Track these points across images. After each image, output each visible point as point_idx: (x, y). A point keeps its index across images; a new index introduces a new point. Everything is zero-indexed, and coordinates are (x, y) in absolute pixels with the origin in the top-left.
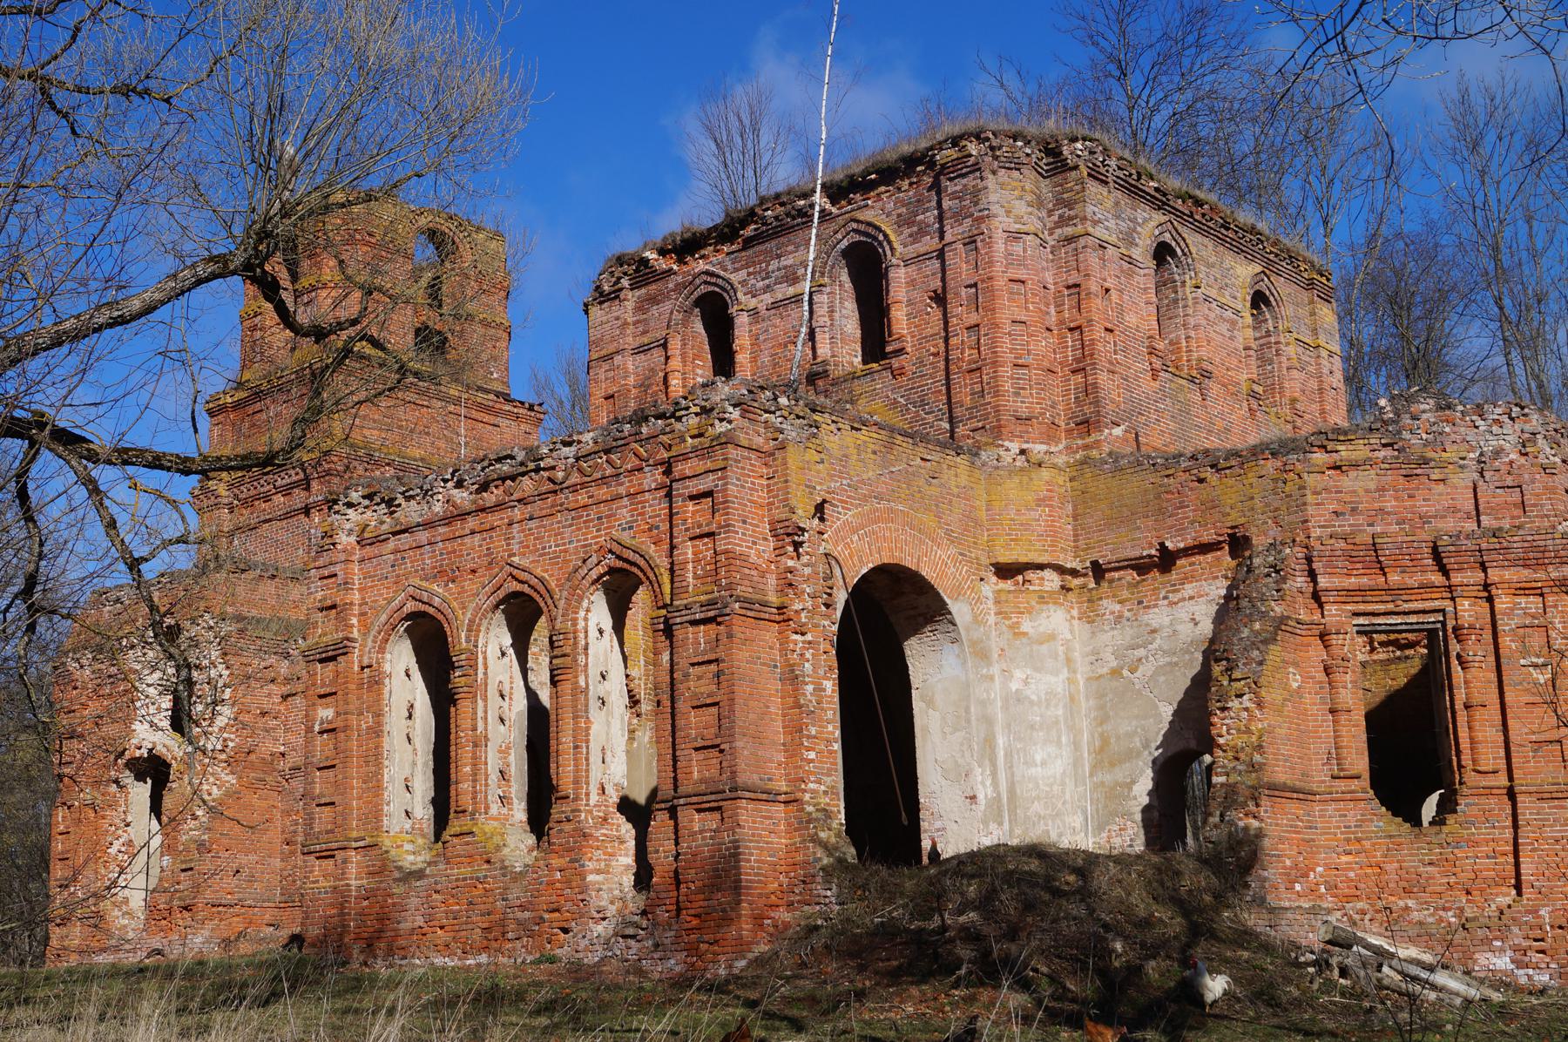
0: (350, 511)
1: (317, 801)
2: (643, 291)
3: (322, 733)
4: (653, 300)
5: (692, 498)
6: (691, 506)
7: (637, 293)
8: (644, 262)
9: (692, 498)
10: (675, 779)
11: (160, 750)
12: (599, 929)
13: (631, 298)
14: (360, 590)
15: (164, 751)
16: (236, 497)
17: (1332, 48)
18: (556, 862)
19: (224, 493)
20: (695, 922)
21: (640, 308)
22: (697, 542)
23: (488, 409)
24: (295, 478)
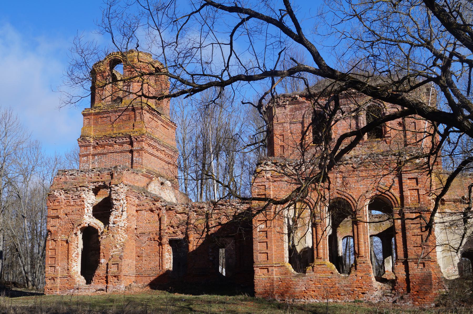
0: (267, 167)
1: (260, 252)
2: (293, 106)
3: (260, 232)
4: (296, 109)
5: (409, 179)
6: (408, 181)
7: (290, 106)
8: (296, 98)
9: (409, 179)
10: (160, 227)
11: (92, 224)
12: (376, 293)
13: (289, 107)
14: (273, 191)
15: (94, 225)
16: (97, 144)
17: (425, 68)
18: (359, 274)
19: (92, 142)
20: (415, 293)
21: (291, 110)
22: (411, 191)
23: (167, 124)
24: (125, 141)
